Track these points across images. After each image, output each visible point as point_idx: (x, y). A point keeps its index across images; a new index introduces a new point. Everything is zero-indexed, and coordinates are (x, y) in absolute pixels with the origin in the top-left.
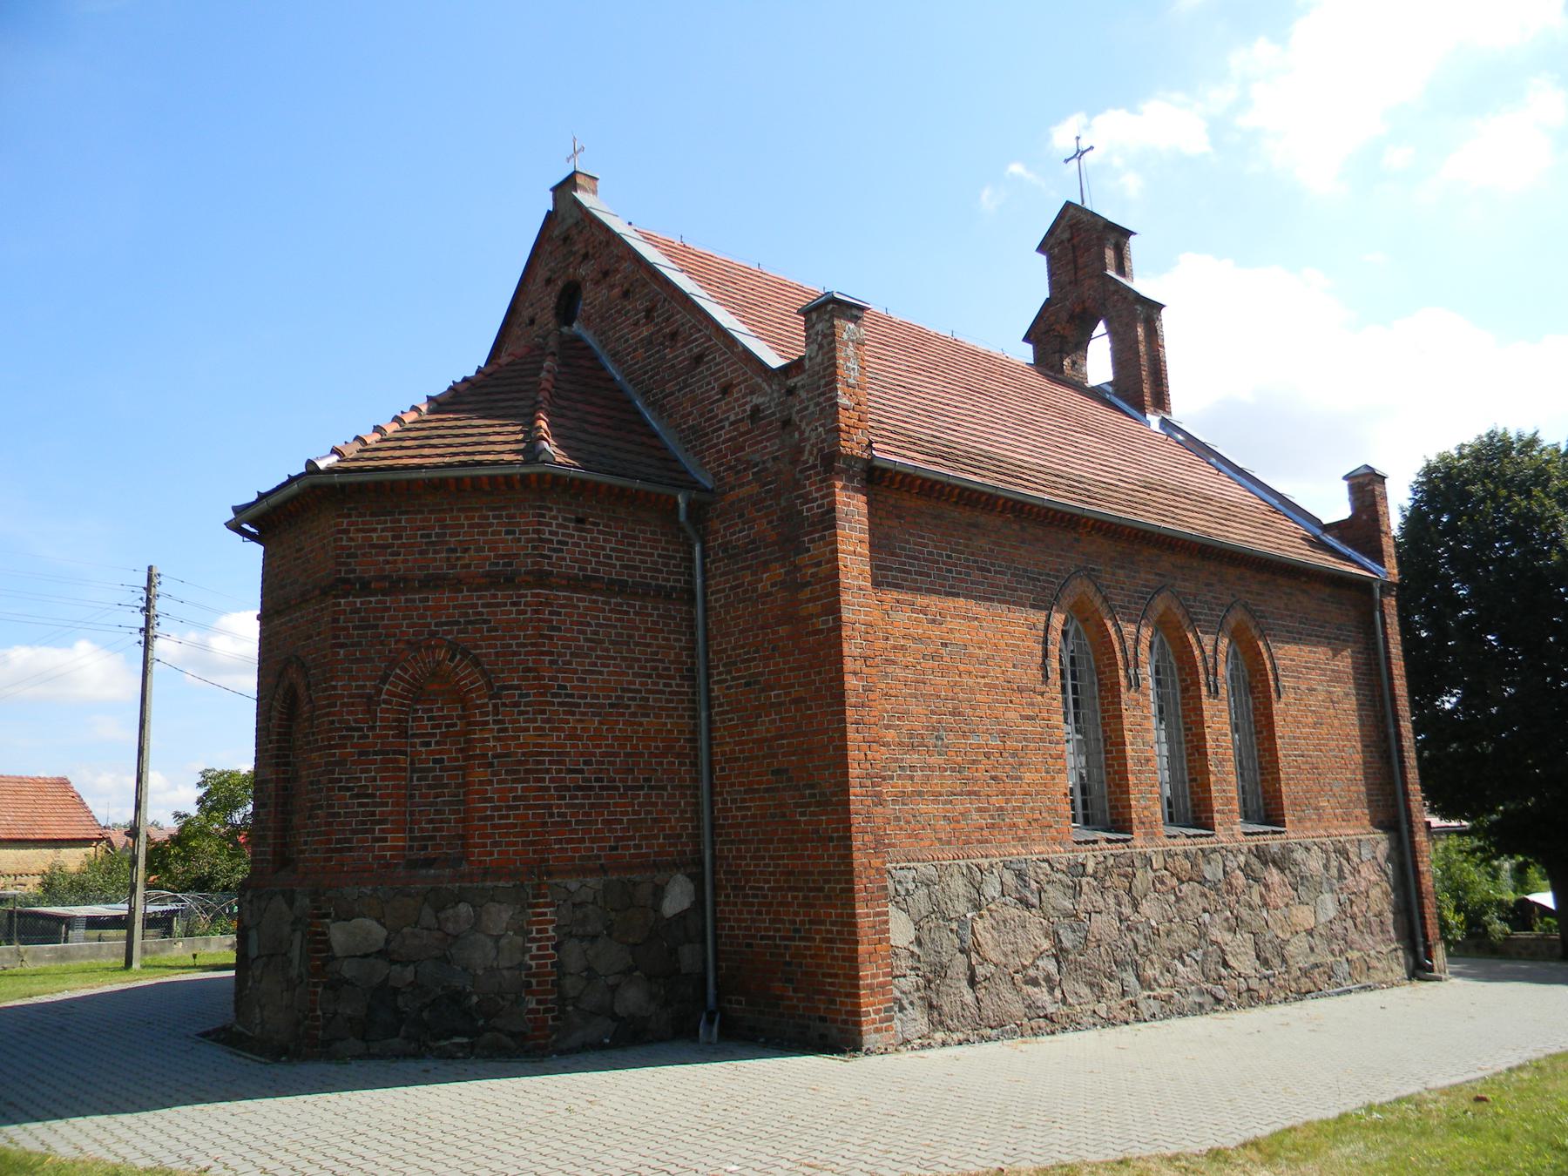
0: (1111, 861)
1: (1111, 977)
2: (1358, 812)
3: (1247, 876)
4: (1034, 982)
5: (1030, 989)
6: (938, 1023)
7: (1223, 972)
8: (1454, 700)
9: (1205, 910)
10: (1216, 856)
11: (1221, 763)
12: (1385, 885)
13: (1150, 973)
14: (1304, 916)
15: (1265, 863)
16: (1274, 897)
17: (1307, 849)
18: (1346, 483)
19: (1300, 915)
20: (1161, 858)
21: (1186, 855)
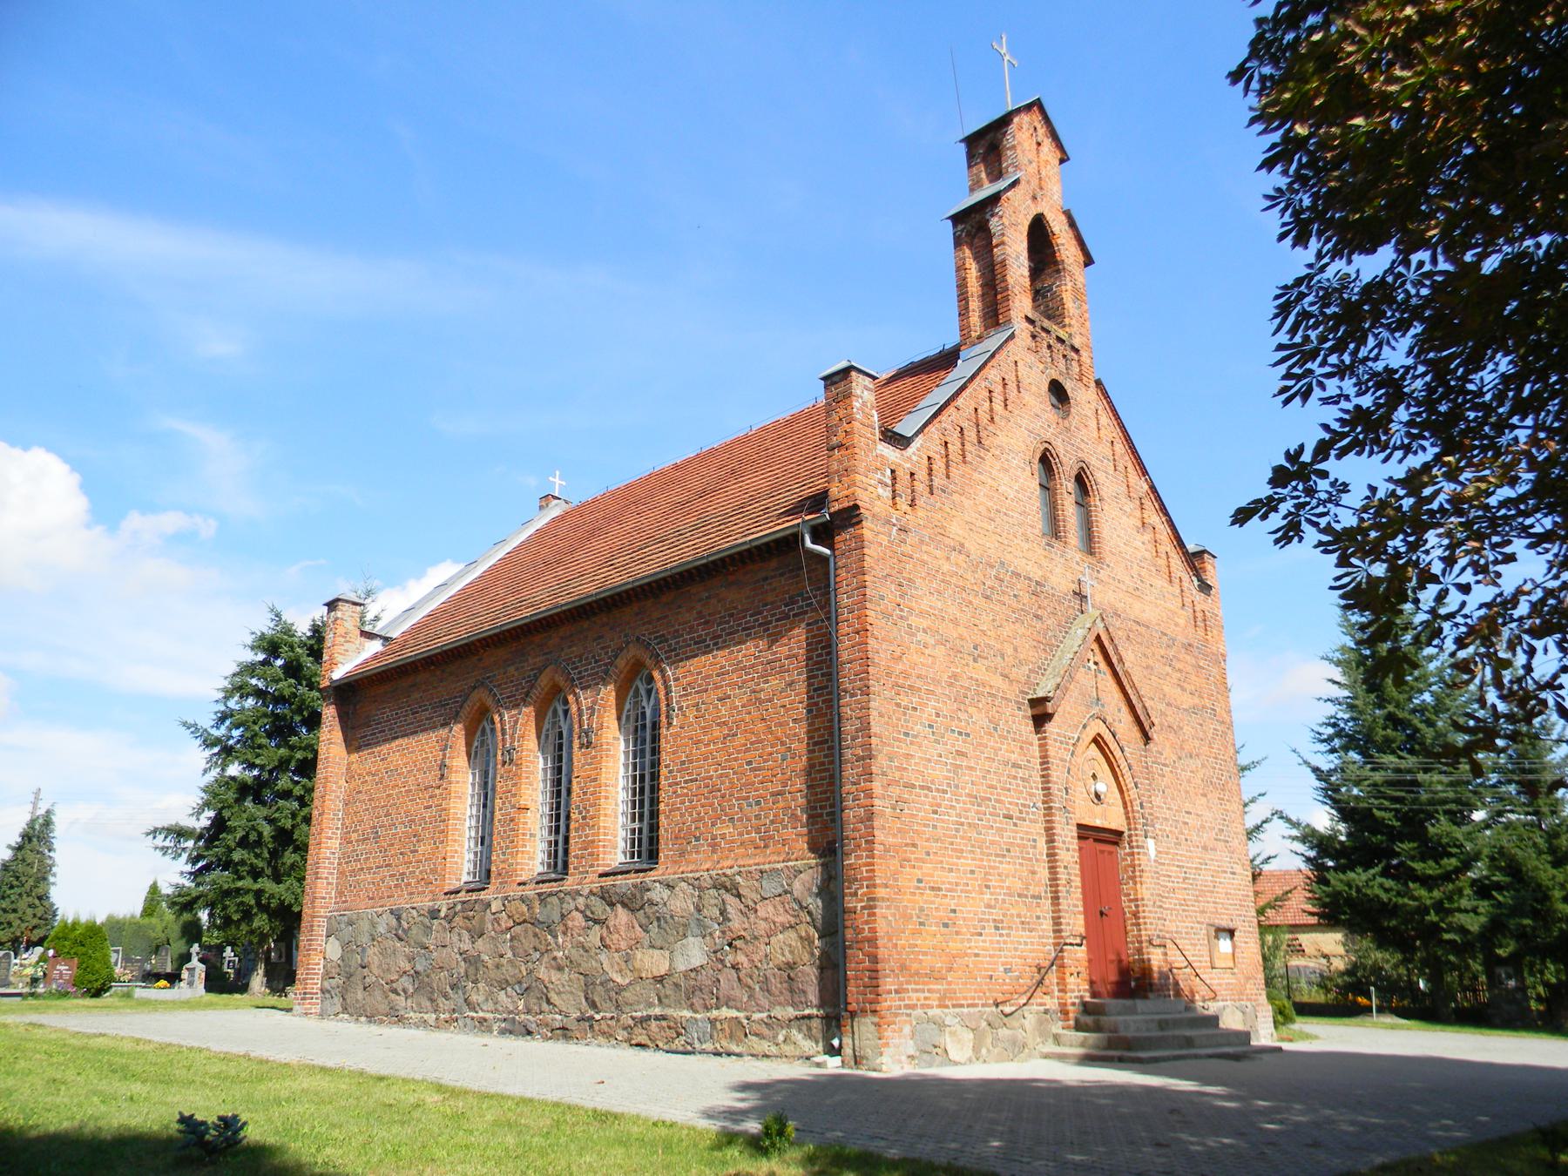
0: (459, 907)
1: (446, 996)
2: (789, 832)
3: (587, 919)
4: (395, 991)
5: (392, 996)
6: (345, 1010)
7: (545, 1006)
8: (1443, 265)
9: (536, 949)
10: (554, 900)
11: (1069, 882)
12: (804, 929)
13: (474, 998)
14: (653, 962)
15: (612, 905)
16: (620, 941)
17: (670, 887)
18: (963, 145)
19: (647, 959)
20: (499, 902)
21: (522, 899)
